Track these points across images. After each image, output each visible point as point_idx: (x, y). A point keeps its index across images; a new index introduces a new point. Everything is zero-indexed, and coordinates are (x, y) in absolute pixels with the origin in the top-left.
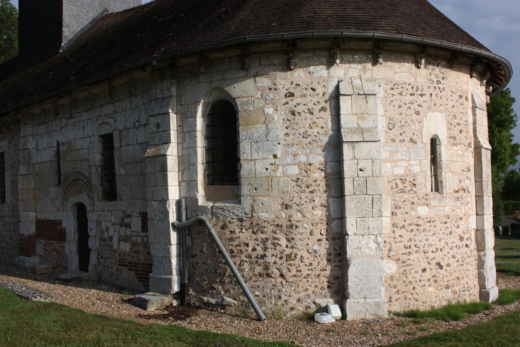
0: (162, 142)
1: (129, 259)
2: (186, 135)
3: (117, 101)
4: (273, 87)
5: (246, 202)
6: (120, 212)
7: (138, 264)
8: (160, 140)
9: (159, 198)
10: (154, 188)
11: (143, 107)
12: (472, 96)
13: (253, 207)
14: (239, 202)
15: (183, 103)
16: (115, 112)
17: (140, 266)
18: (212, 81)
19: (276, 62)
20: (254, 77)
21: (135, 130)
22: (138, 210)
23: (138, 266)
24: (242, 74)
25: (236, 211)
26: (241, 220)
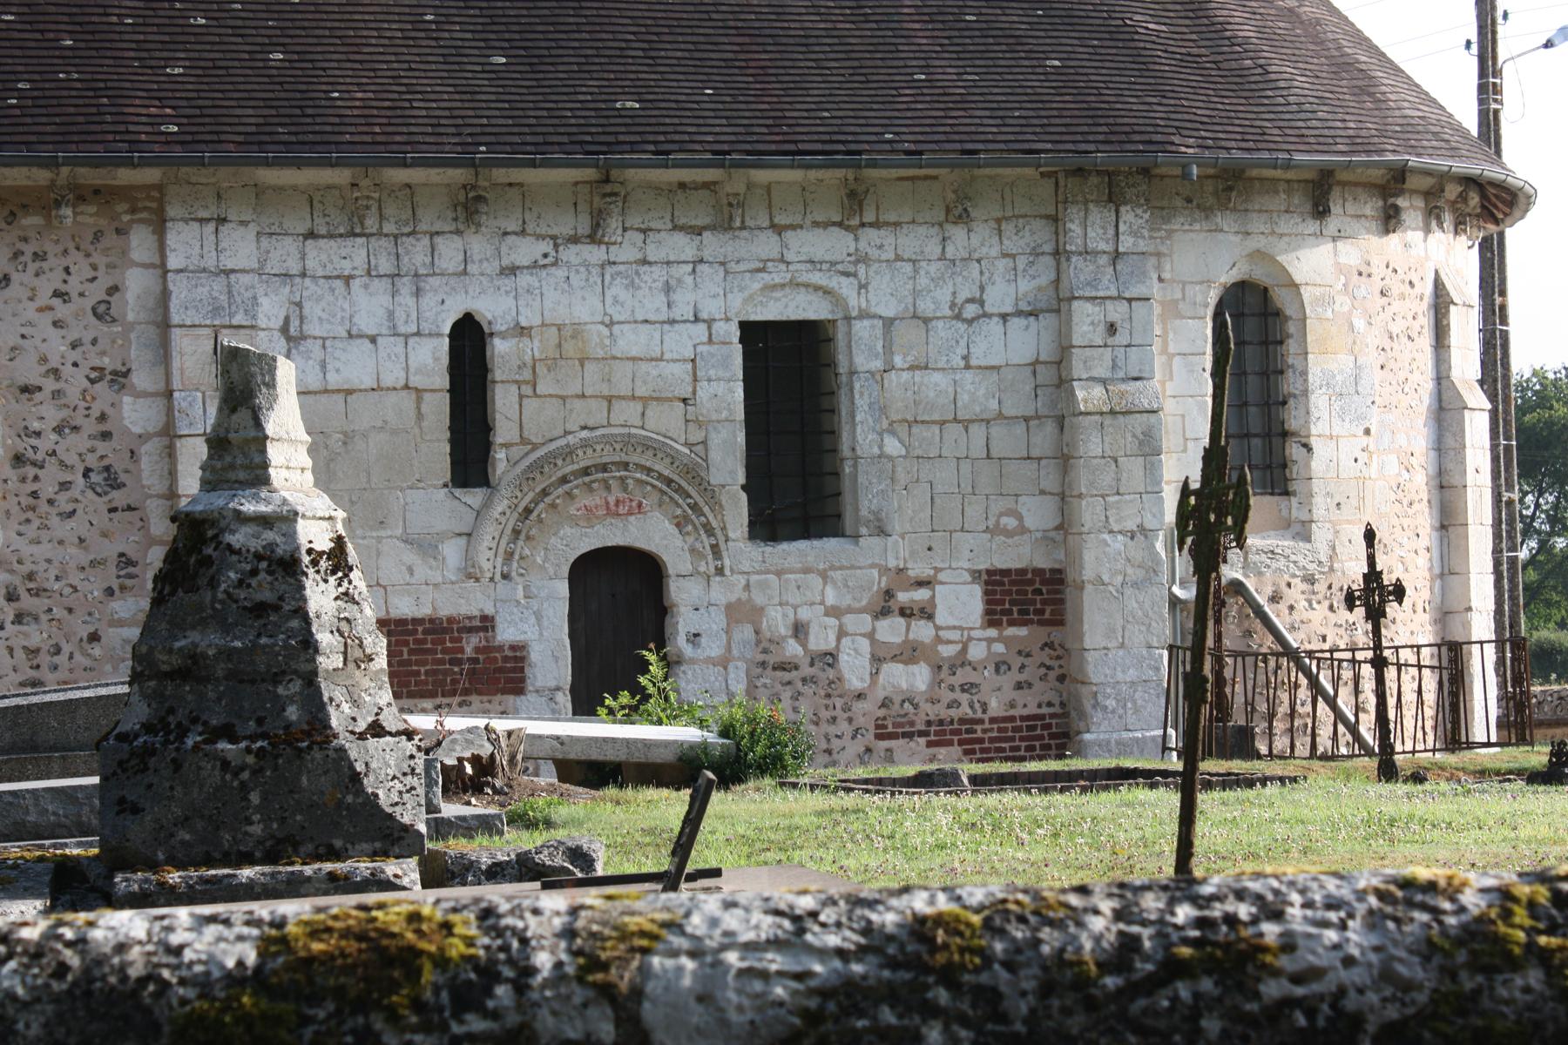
0: (1121, 374)
1: (933, 712)
2: (1177, 360)
3: (876, 225)
4: (1364, 269)
5: (1321, 534)
6: (875, 573)
7: (981, 721)
8: (1114, 366)
9: (1131, 525)
10: (1111, 499)
11: (1002, 264)
12: (935, 178)
13: (1334, 548)
14: (1307, 538)
15: (1166, 275)
16: (864, 259)
17: (987, 726)
18: (1248, 234)
19: (1368, 211)
20: (1334, 239)
21: (962, 327)
22: (966, 565)
23: (979, 728)
24: (1312, 226)
25: (1299, 558)
26: (1310, 580)
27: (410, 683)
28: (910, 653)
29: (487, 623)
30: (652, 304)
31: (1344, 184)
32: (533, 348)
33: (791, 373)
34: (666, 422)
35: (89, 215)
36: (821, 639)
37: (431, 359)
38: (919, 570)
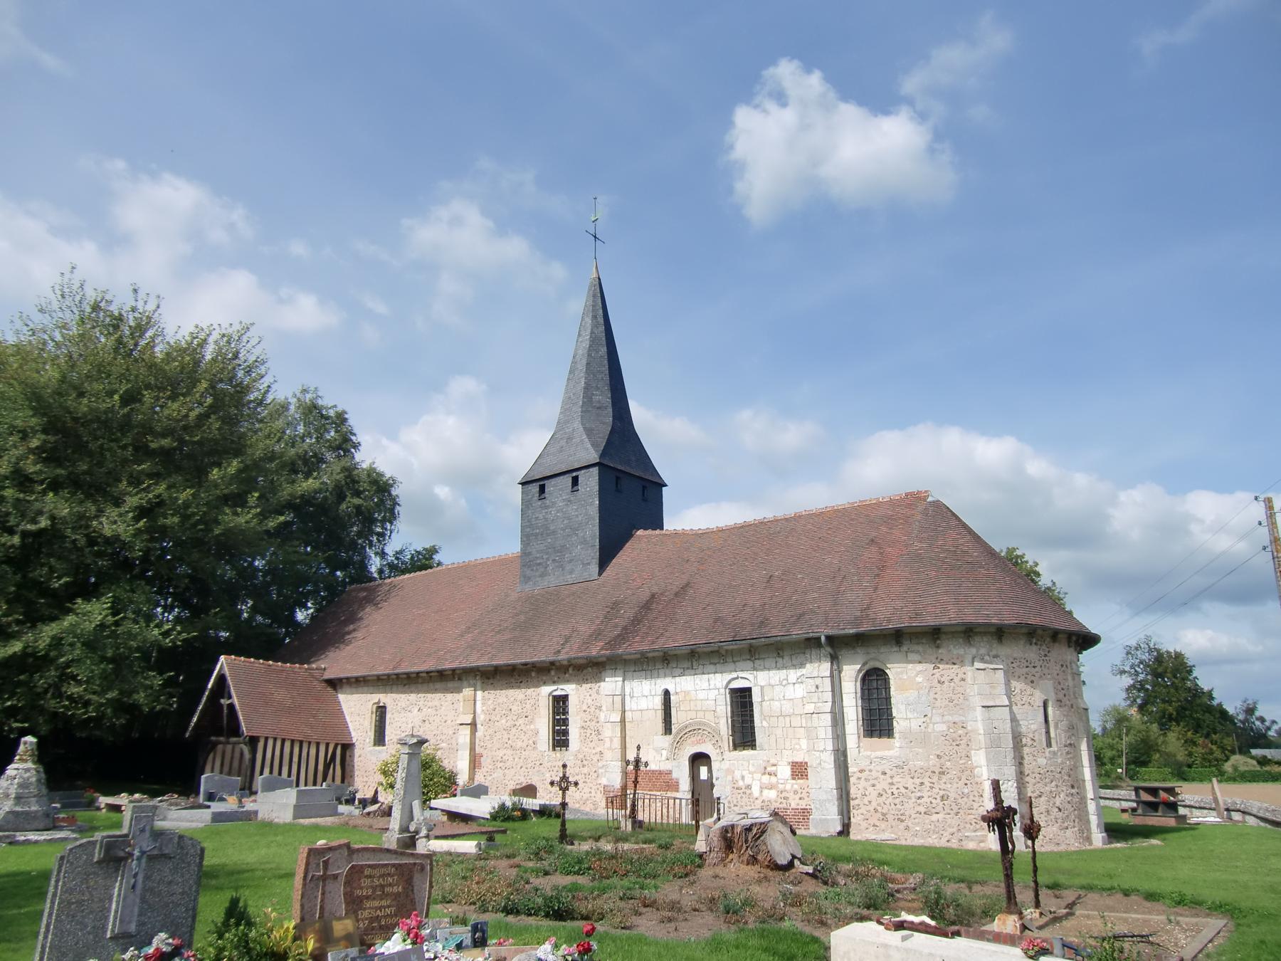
24: (896, 649)
27: (120, 806)
28: (771, 787)
29: (670, 772)
30: (705, 685)
31: (945, 633)
32: (681, 697)
33: (742, 700)
34: (709, 718)
35: (595, 670)
36: (748, 781)
37: (658, 702)
38: (773, 761)
